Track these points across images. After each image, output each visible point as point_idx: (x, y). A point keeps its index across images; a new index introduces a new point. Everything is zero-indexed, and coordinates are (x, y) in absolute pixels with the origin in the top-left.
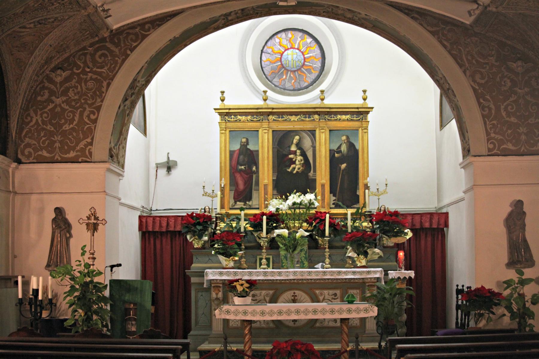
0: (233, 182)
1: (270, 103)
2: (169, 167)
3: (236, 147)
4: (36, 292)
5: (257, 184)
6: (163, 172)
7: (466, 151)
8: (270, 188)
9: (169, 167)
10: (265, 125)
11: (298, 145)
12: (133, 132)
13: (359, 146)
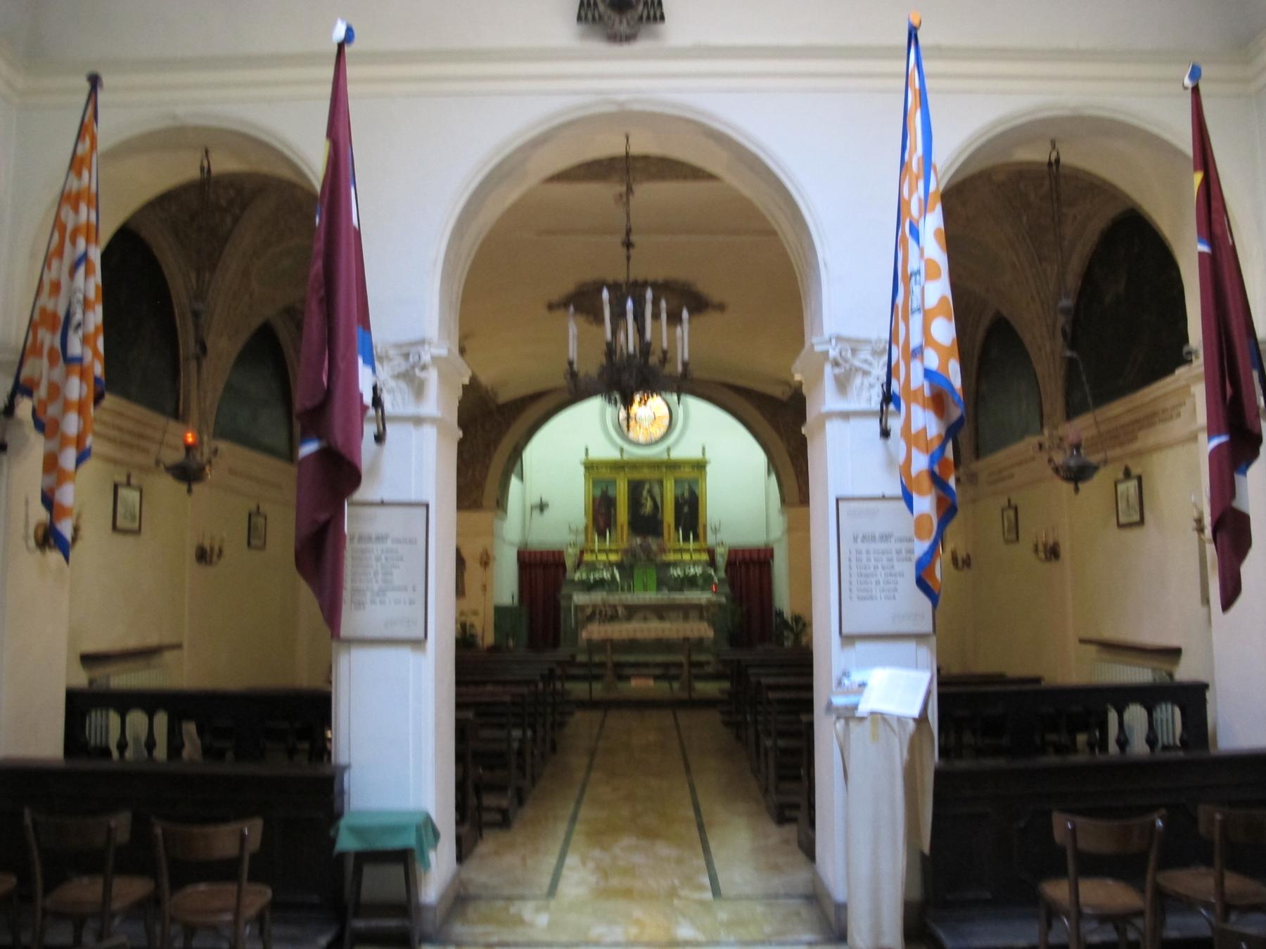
0: (595, 520)
1: (626, 457)
2: (542, 507)
3: (598, 493)
4: (1012, 476)
5: (615, 522)
6: (536, 513)
7: (783, 501)
8: (626, 527)
9: (542, 507)
10: (622, 474)
11: (650, 492)
12: (514, 481)
13: (698, 492)
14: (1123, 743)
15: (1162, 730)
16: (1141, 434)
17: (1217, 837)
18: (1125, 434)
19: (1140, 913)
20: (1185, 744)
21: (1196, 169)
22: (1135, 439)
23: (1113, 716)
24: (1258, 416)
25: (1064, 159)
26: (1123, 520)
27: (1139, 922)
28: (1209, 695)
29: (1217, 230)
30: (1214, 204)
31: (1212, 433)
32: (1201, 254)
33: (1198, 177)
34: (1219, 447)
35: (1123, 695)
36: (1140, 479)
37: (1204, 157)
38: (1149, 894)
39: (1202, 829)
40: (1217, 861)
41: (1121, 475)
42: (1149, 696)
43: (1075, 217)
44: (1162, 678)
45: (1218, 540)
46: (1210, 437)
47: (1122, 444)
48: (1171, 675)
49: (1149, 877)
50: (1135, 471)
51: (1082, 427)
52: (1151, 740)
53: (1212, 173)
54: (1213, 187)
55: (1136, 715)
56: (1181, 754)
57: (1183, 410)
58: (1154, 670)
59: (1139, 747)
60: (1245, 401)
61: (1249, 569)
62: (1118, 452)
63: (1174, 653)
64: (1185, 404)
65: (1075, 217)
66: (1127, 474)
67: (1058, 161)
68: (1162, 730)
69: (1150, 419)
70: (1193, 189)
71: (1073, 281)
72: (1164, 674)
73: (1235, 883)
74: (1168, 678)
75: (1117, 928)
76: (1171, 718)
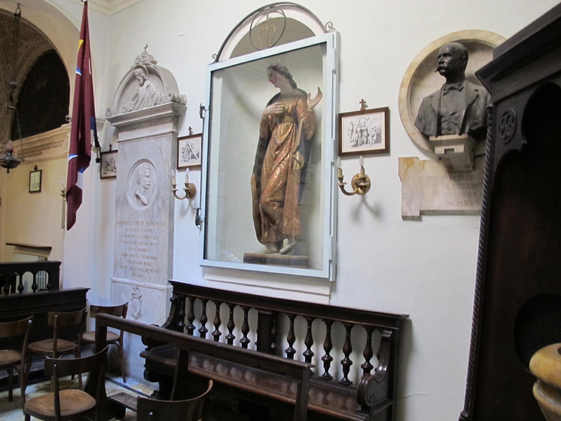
14: (21, 289)
15: (40, 282)
16: (44, 151)
17: (55, 325)
18: (36, 151)
19: (18, 362)
20: (49, 287)
21: (80, 39)
22: (41, 153)
23: (18, 277)
24: (90, 148)
25: (23, 15)
26: (31, 190)
27: (19, 367)
28: (61, 267)
29: (85, 67)
30: (86, 56)
31: (71, 153)
32: (77, 74)
33: (81, 41)
34: (73, 159)
35: (23, 268)
36: (41, 171)
37: (85, 34)
38: (23, 354)
39: (49, 322)
40: (55, 336)
41: (33, 170)
42: (34, 268)
43: (27, 47)
44: (42, 259)
45: (68, 199)
46: (70, 156)
47: (35, 155)
48: (46, 259)
49: (24, 346)
50: (39, 168)
51: (17, 145)
52: (34, 287)
53: (87, 42)
54: (87, 47)
55: (28, 276)
56: (47, 291)
57: (63, 143)
58: (39, 256)
59: (29, 290)
60: (86, 142)
61: (80, 213)
62: (33, 158)
63: (48, 249)
64: (64, 141)
65: (27, 47)
66: (36, 169)
67: (19, 14)
68: (40, 282)
69: (47, 146)
70: (78, 47)
71: (21, 77)
72: (43, 258)
73: (61, 343)
74: (45, 260)
75: (8, 371)
76: (43, 277)
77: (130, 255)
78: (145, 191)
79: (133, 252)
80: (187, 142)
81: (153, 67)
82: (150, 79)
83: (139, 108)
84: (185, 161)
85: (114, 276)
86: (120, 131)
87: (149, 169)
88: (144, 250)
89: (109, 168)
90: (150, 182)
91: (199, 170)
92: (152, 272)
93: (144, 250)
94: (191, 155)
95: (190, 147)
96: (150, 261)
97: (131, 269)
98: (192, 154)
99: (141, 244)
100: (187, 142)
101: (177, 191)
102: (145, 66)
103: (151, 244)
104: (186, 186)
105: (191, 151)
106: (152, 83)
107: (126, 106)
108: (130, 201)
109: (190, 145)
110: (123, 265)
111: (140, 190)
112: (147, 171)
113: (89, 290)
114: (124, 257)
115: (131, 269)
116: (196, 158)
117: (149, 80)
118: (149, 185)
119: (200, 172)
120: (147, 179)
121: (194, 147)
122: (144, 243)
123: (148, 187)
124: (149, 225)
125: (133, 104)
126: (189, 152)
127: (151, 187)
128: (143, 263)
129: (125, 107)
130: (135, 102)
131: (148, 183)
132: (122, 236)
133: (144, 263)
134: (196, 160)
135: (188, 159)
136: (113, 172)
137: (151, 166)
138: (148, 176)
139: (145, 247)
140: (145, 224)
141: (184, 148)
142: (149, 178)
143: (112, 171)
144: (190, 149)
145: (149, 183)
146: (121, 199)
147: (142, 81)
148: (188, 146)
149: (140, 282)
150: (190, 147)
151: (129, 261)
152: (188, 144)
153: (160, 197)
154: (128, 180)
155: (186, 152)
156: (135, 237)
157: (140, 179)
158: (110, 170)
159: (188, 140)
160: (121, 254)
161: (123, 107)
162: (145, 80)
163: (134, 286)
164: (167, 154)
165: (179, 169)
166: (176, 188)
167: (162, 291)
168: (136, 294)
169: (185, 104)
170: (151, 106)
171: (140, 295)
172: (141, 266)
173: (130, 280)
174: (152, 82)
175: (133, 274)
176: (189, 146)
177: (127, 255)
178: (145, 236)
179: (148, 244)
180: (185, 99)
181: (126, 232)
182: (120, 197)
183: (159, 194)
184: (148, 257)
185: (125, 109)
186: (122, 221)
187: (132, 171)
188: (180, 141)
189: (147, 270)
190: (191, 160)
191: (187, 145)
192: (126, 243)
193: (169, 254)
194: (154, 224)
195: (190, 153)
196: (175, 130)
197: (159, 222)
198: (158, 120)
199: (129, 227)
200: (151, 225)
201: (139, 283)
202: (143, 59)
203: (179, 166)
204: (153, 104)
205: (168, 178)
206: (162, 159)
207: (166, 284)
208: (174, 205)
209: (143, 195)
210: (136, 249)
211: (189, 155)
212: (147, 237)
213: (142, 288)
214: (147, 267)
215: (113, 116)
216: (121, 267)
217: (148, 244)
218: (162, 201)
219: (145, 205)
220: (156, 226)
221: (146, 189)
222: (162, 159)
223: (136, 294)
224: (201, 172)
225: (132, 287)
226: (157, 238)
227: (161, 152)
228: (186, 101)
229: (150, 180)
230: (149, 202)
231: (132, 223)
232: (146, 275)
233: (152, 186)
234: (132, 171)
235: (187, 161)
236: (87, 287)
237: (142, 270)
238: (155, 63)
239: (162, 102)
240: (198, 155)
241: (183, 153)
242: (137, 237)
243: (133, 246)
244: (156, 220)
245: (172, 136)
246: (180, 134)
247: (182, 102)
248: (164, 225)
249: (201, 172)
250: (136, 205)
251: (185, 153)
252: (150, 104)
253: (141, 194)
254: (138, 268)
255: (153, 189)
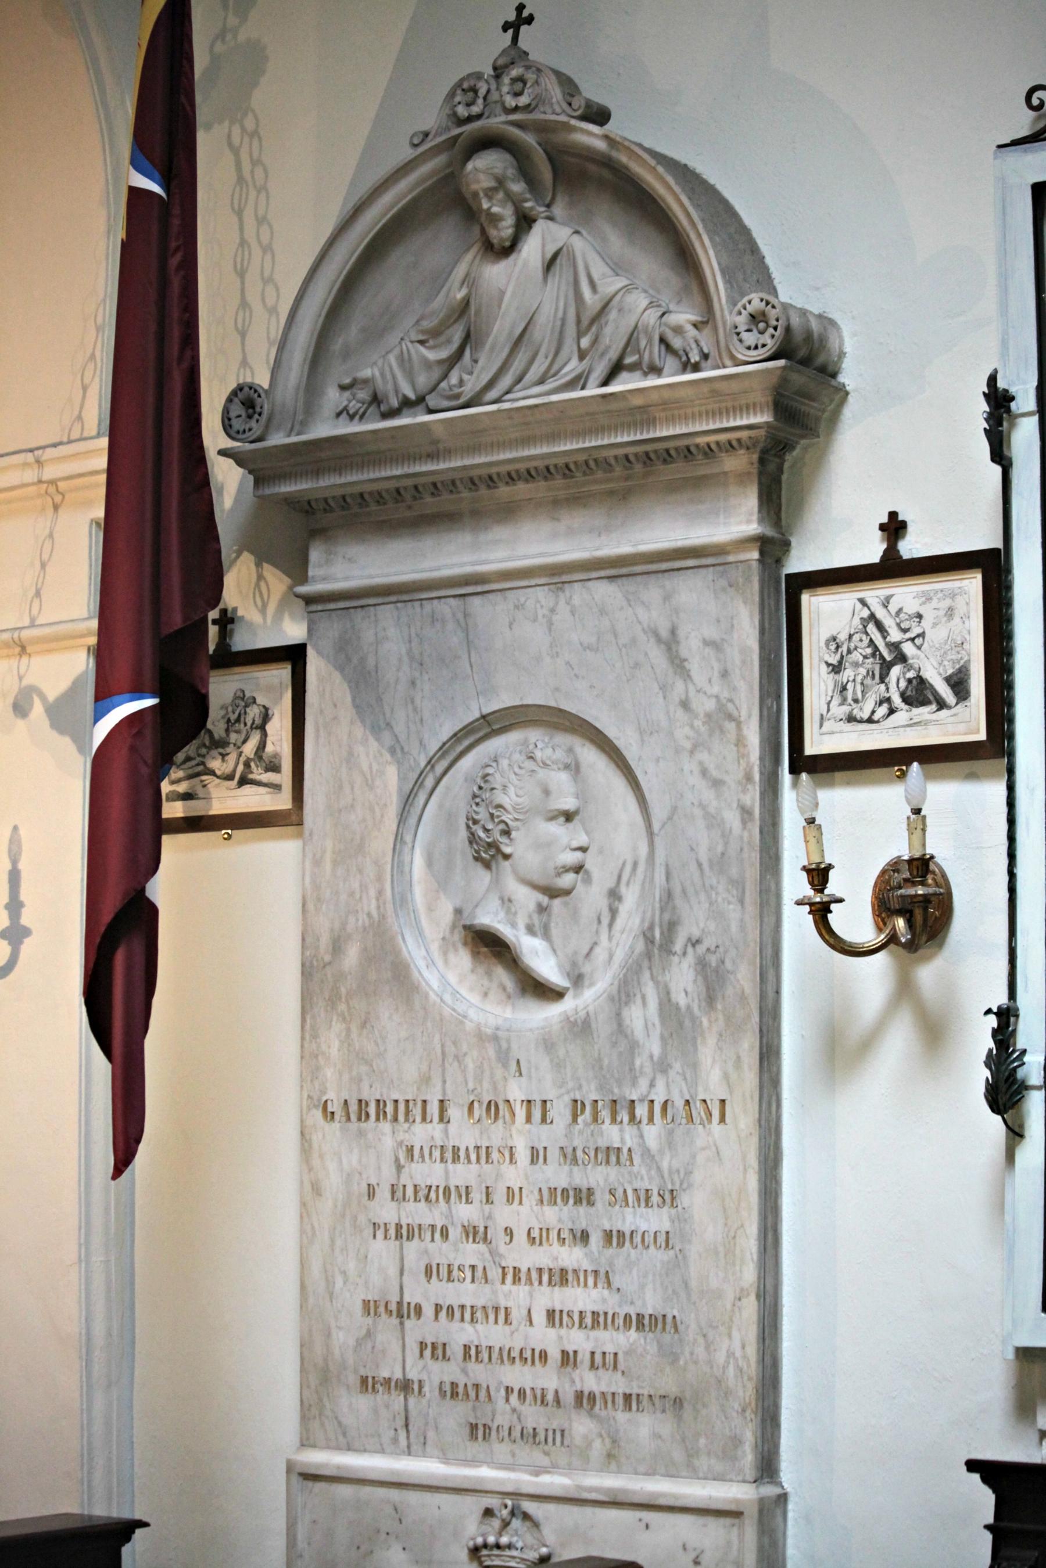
77: (438, 1308)
78: (542, 909)
79: (466, 1293)
80: (863, 602)
81: (601, 145)
82: (558, 210)
83: (493, 394)
84: (851, 719)
85: (306, 1442)
86: (317, 533)
87: (574, 768)
88: (562, 1277)
89: (215, 764)
90: (583, 849)
91: (992, 776)
92: (628, 1406)
93: (562, 1277)
94: (903, 684)
95: (895, 636)
96: (610, 1340)
97: (453, 1392)
98: (911, 675)
99: (532, 1241)
100: (863, 602)
101: (833, 907)
102: (529, 139)
103: (613, 1238)
104: (812, 883)
105: (902, 658)
106: (576, 237)
107: (366, 373)
108: (426, 974)
109: (889, 623)
110: (386, 1374)
111: (507, 902)
112: (561, 779)
113: (139, 1533)
114: (395, 1321)
115: (453, 1392)
116: (942, 705)
117: (551, 218)
118: (578, 869)
119: (999, 789)
120: (557, 829)
121: (922, 635)
122: (553, 1235)
123: (567, 880)
124: (595, 1119)
125: (428, 365)
126: (886, 667)
127: (588, 880)
128: (554, 1354)
129: (366, 381)
130: (444, 354)
131: (572, 858)
132: (371, 1192)
133: (564, 1353)
134: (944, 713)
135: (883, 710)
136: (248, 789)
137: (590, 756)
138: (569, 817)
139: (571, 1257)
140: (560, 1111)
141: (843, 637)
142: (570, 825)
143: (244, 781)
144: (895, 647)
145: (579, 855)
146: (352, 956)
147: (506, 229)
148: (871, 628)
149: (537, 1474)
150: (895, 636)
151: (438, 1351)
152: (872, 617)
153: (678, 947)
154: (398, 838)
155: (856, 665)
156: (477, 1196)
157: (507, 833)
158: (230, 777)
159: (874, 593)
160: (366, 1303)
161: (347, 381)
162: (525, 222)
163: (493, 1502)
164: (725, 674)
165: (801, 763)
166: (833, 888)
167: (728, 1521)
168: (510, 1546)
169: (830, 369)
170: (579, 381)
171: (544, 1550)
172: (548, 1379)
173: (445, 1460)
174: (577, 232)
175: (473, 1427)
176: (880, 626)
177: (419, 1310)
178: (564, 1191)
179: (595, 1239)
180: (833, 343)
181: (399, 1168)
182: (337, 947)
183: (671, 927)
184: (597, 1320)
185: (363, 395)
186: (365, 1096)
187: (429, 782)
188: (808, 600)
189: (584, 1400)
190: (904, 715)
191: (865, 622)
192: (403, 1233)
193: (761, 1295)
194: (641, 1111)
195: (896, 671)
196: (770, 532)
197: (679, 1103)
198: (638, 467)
199: (421, 1134)
200: (614, 1120)
201: (526, 1477)
202: (517, 94)
203: (809, 750)
204: (600, 370)
205: (744, 822)
206: (685, 705)
207: (750, 1477)
208: (778, 992)
209: (531, 930)
210: (494, 1273)
211: (882, 680)
212: (583, 1196)
213: (551, 1507)
214: (591, 1382)
215: (277, 439)
216: (366, 1384)
217: (595, 1239)
218: (702, 965)
219: (553, 994)
220: (651, 1119)
221: (553, 893)
222: (685, 705)
223: (510, 1546)
224: (1011, 788)
225: (473, 1506)
226: (670, 1197)
227: (679, 665)
228: (842, 355)
229: (582, 840)
230: (578, 980)
231: (453, 1112)
232: (581, 1426)
233: (601, 875)
234: (429, 782)
235: (870, 721)
236: (126, 1514)
237: (550, 1397)
238: (599, 116)
239: (671, 363)
240: (959, 684)
241: (836, 669)
242: (499, 1196)
243: (471, 1253)
244: (652, 1085)
245: (755, 565)
246: (794, 552)
247: (820, 360)
248: (722, 1119)
249: (1011, 788)
250: (474, 998)
251: (848, 674)
252: (573, 367)
253: (514, 925)
254: (509, 1390)
255: (614, 895)
